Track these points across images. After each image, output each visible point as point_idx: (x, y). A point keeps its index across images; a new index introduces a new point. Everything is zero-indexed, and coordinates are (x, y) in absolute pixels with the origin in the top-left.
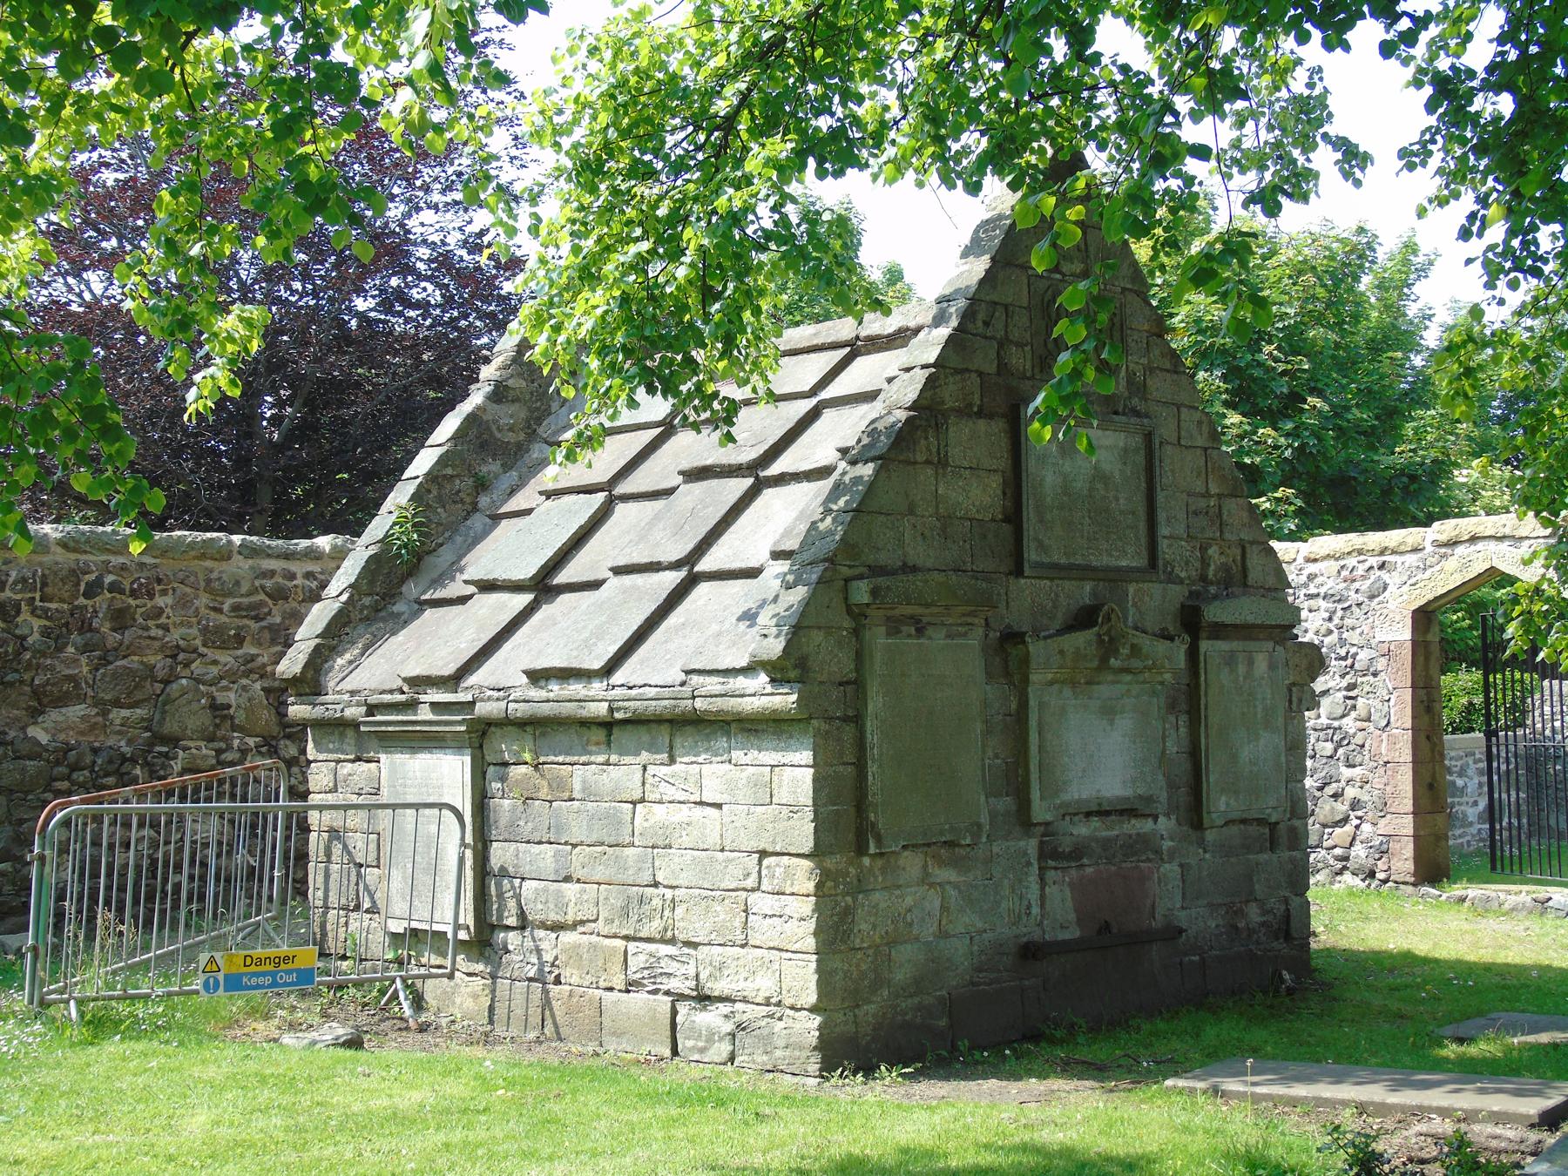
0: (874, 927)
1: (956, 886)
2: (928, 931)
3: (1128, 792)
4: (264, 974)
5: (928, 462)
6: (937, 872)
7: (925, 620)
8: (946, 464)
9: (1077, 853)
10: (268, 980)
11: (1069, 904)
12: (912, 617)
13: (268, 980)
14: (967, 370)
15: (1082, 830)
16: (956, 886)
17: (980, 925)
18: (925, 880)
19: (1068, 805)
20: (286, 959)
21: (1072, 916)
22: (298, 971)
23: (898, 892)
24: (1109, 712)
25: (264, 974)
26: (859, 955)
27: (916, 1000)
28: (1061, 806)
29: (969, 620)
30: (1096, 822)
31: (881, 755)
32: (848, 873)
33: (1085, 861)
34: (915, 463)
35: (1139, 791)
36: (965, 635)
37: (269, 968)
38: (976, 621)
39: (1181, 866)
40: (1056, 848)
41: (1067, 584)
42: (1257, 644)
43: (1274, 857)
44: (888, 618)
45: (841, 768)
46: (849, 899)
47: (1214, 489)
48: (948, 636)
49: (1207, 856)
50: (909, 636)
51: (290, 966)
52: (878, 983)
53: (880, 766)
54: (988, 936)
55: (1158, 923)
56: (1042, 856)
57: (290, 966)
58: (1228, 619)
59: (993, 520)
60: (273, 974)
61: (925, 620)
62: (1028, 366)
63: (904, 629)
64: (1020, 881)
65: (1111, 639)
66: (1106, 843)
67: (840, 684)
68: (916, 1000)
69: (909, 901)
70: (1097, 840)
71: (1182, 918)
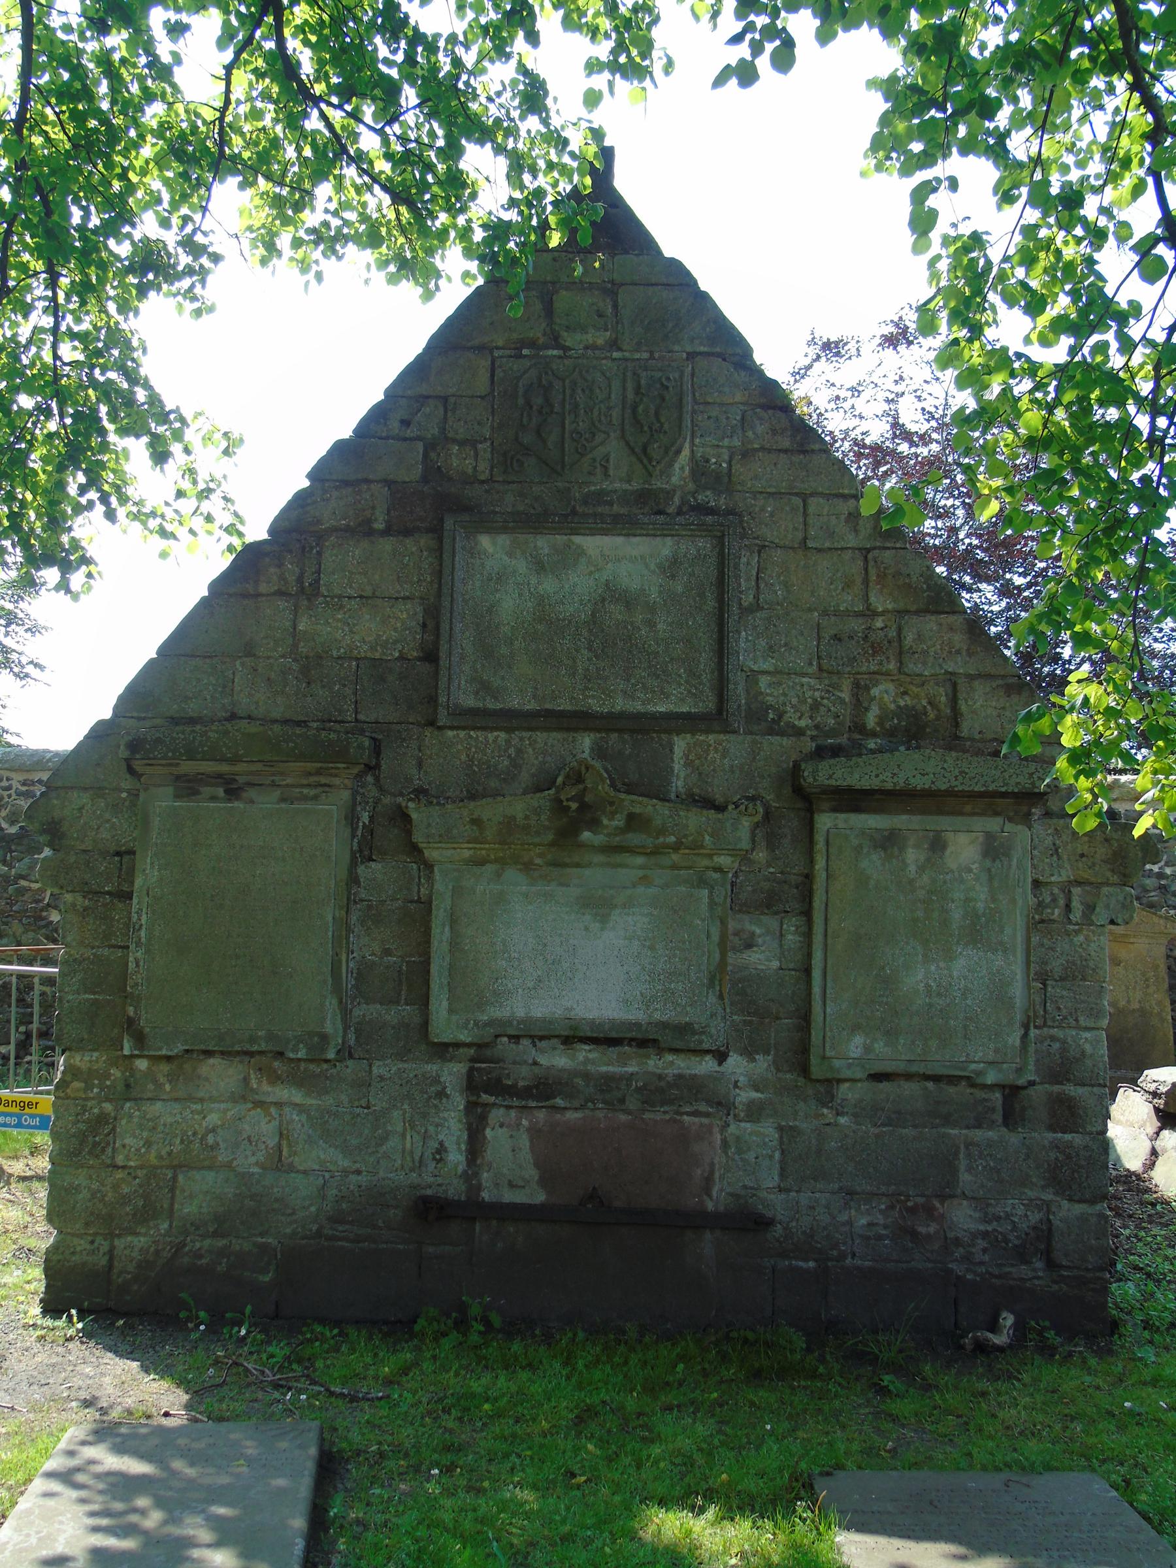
0: (148, 1144)
1: (300, 1108)
2: (249, 1161)
3: (636, 1014)
4: (11, 1115)
5: (280, 593)
6: (266, 1087)
7: (241, 780)
8: (318, 594)
9: (544, 1089)
10: (14, 1120)
11: (526, 1155)
12: (220, 776)
13: (14, 1120)
14: (367, 481)
15: (558, 1060)
16: (300, 1108)
17: (345, 1163)
18: (245, 1094)
19: (509, 1022)
20: (30, 1104)
21: (532, 1173)
22: (41, 1116)
23: (198, 1107)
24: (599, 907)
25: (11, 1115)
26: (120, 1174)
27: (221, 1243)
28: (490, 1023)
29: (323, 780)
30: (584, 1053)
31: (149, 940)
32: (107, 1076)
33: (559, 1101)
34: (259, 595)
35: (657, 1016)
36: (315, 798)
37: (17, 1110)
38: (337, 781)
39: (780, 1129)
40: (499, 1080)
41: (540, 736)
42: (959, 820)
43: (1014, 1139)
44: (178, 778)
45: (106, 952)
46: (108, 1107)
47: (880, 602)
48: (283, 800)
49: (842, 1120)
50: (213, 798)
51: (33, 1111)
52: (146, 1214)
53: (148, 952)
54: (363, 1179)
55: (717, 1200)
56: (472, 1085)
57: (33, 1111)
58: (866, 783)
59: (402, 657)
60: (19, 1116)
61: (241, 780)
62: (483, 466)
63: (207, 791)
64: (425, 1116)
65: (584, 807)
66: (607, 1083)
67: (118, 854)
68: (221, 1243)
69: (213, 1119)
70: (586, 1076)
71: (776, 1204)
